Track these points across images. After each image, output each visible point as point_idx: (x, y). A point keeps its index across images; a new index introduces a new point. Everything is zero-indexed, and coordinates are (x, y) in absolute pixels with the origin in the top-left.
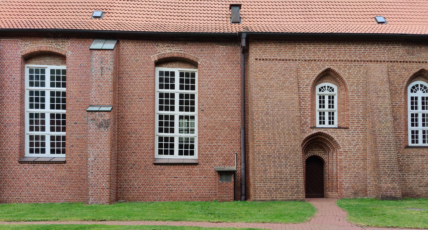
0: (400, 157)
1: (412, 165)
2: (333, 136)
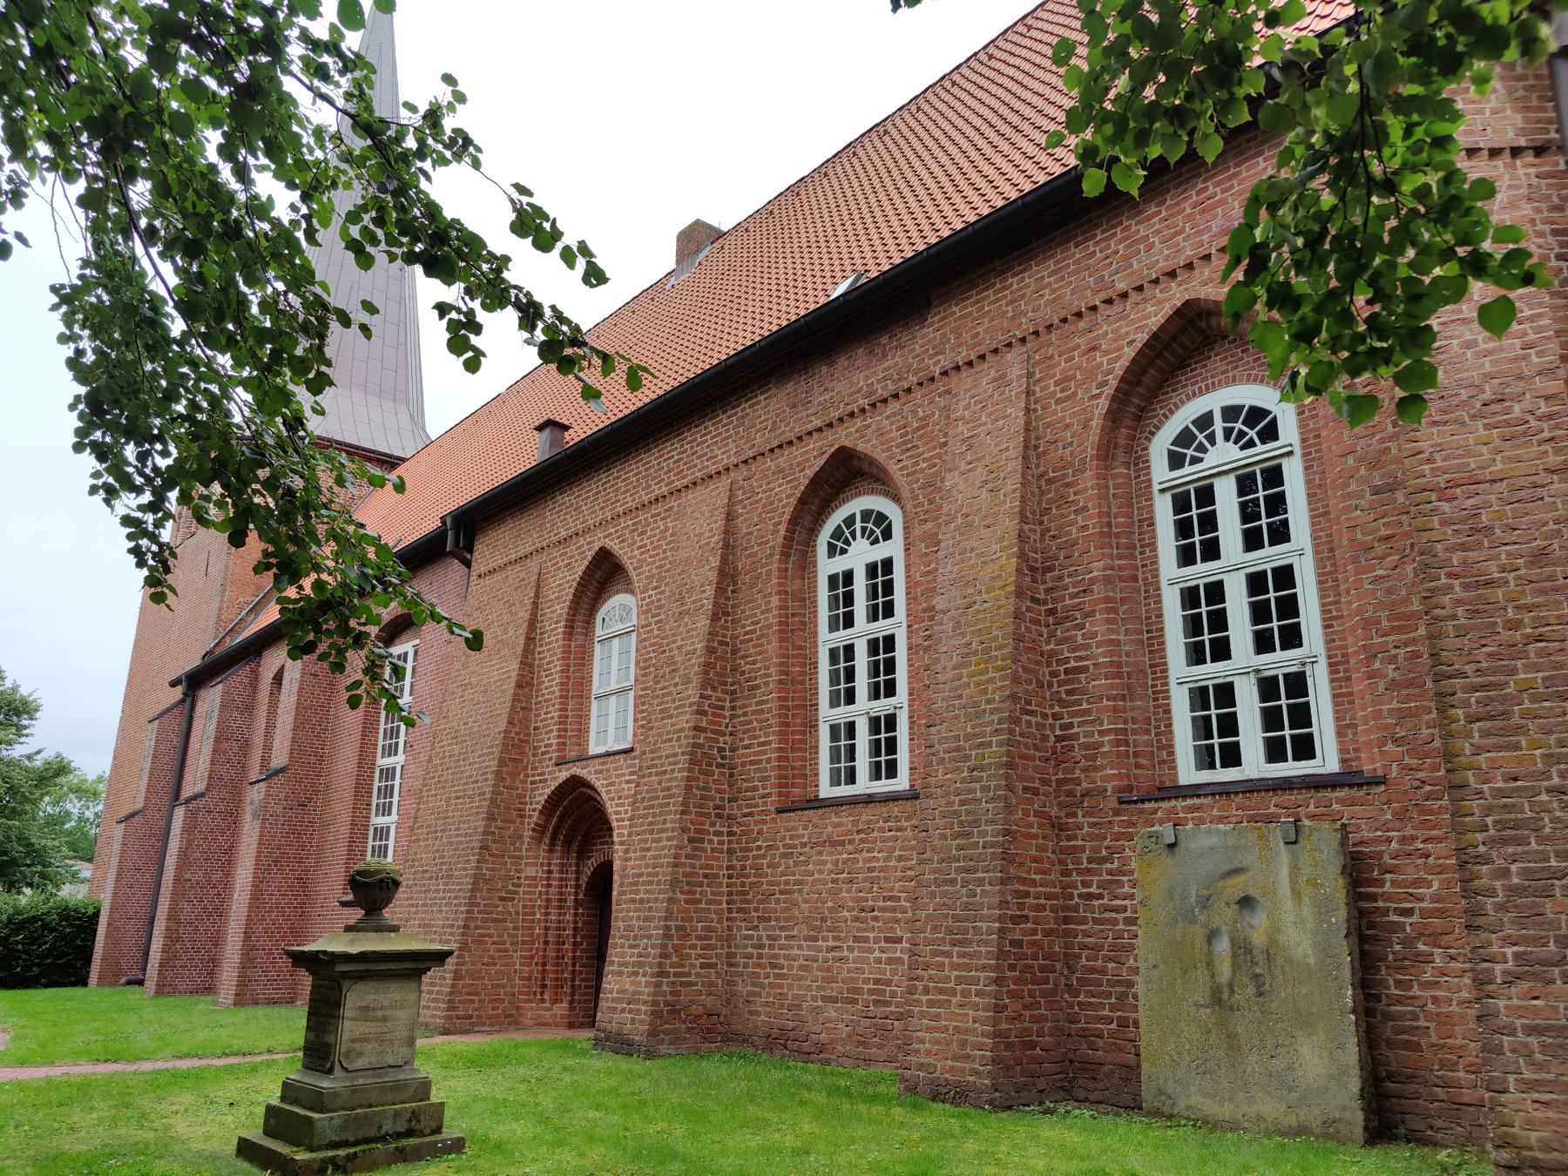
0: (763, 857)
2: (597, 784)
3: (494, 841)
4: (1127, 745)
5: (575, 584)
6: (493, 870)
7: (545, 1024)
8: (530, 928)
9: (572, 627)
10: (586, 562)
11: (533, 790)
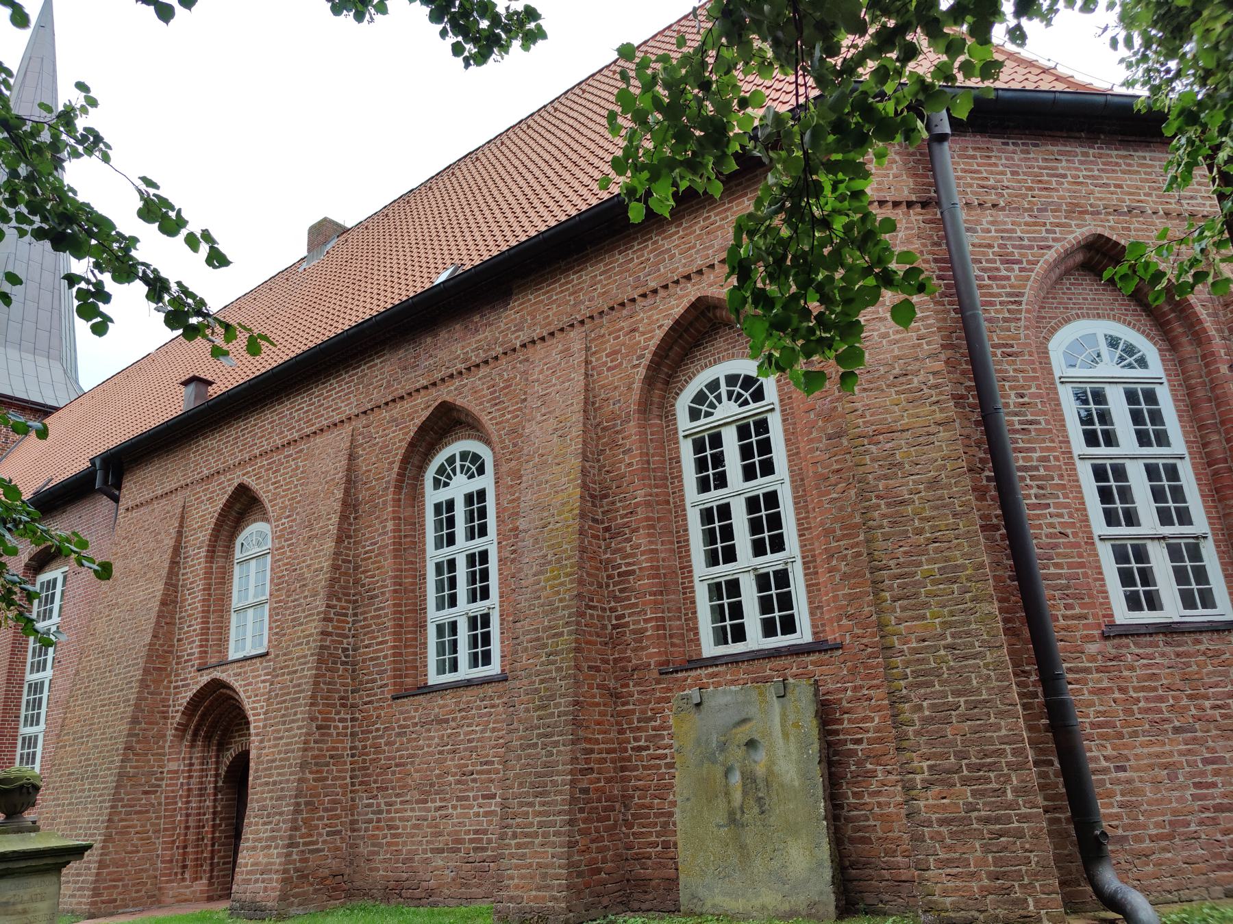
0: (381, 737)
1: (412, 763)
2: (236, 685)
3: (138, 742)
4: (665, 629)
5: (216, 515)
6: (136, 767)
7: (185, 901)
8: (171, 816)
9: (214, 552)
10: (226, 496)
11: (176, 694)
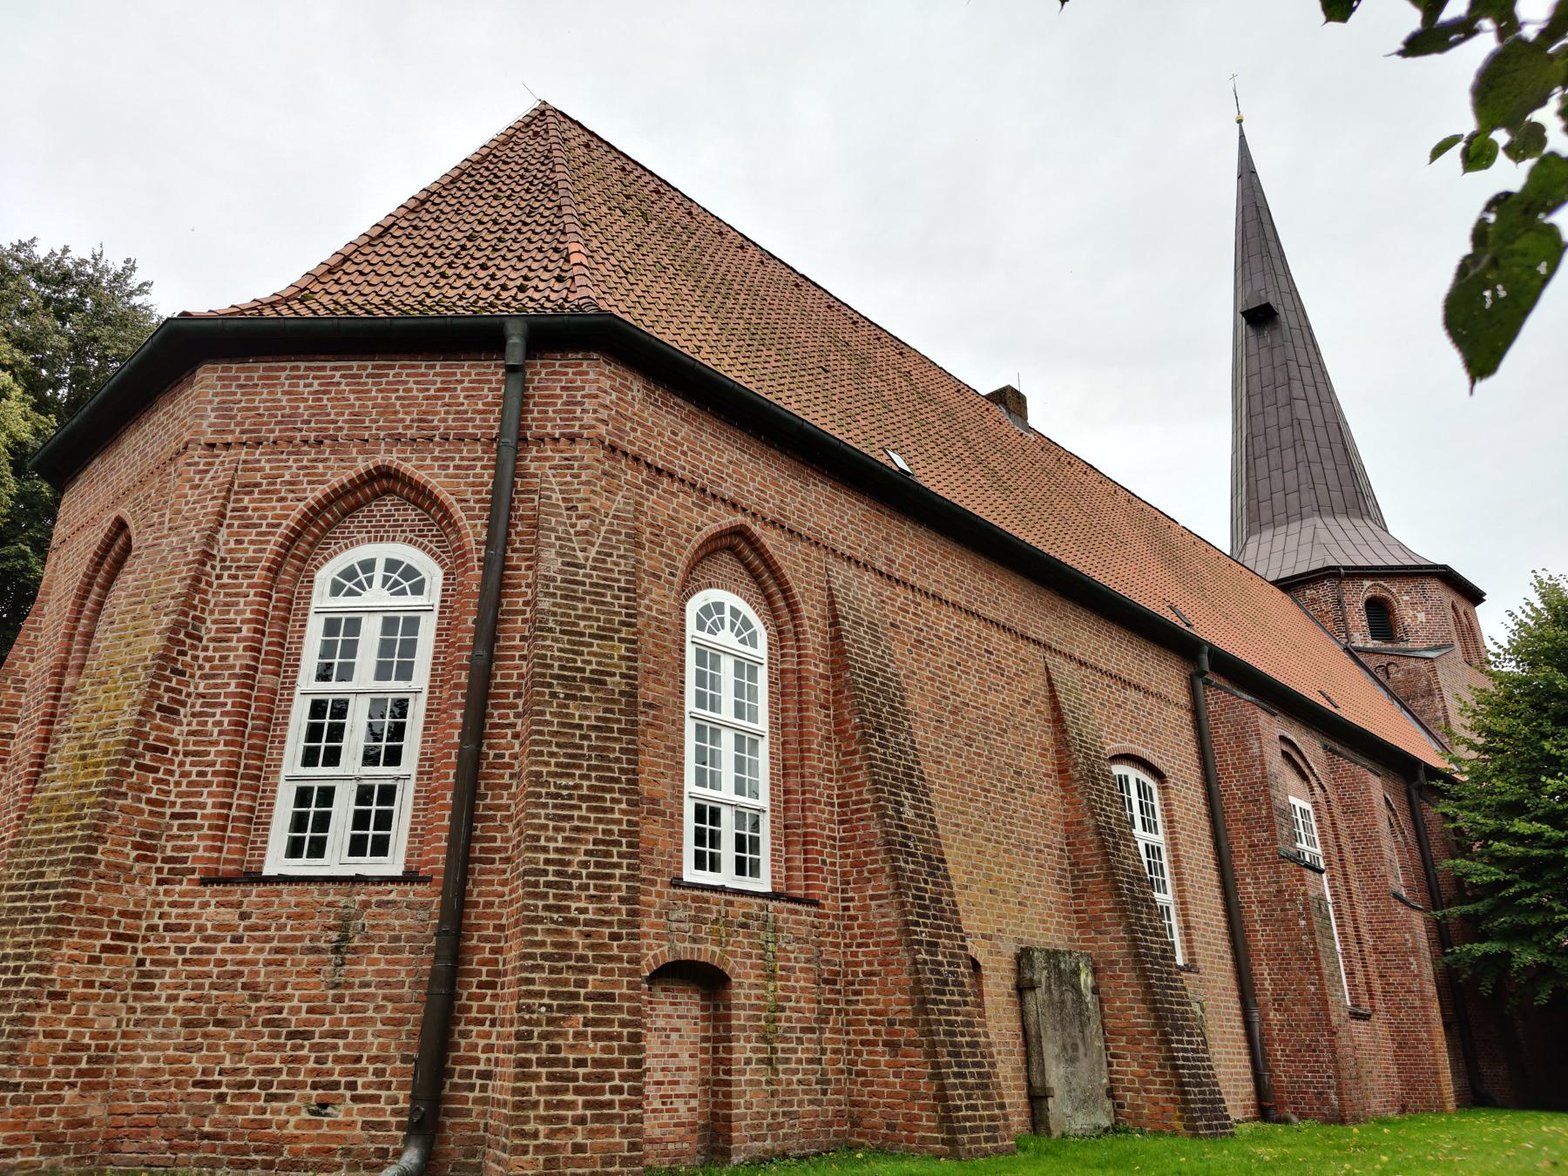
4: (252, 689)
